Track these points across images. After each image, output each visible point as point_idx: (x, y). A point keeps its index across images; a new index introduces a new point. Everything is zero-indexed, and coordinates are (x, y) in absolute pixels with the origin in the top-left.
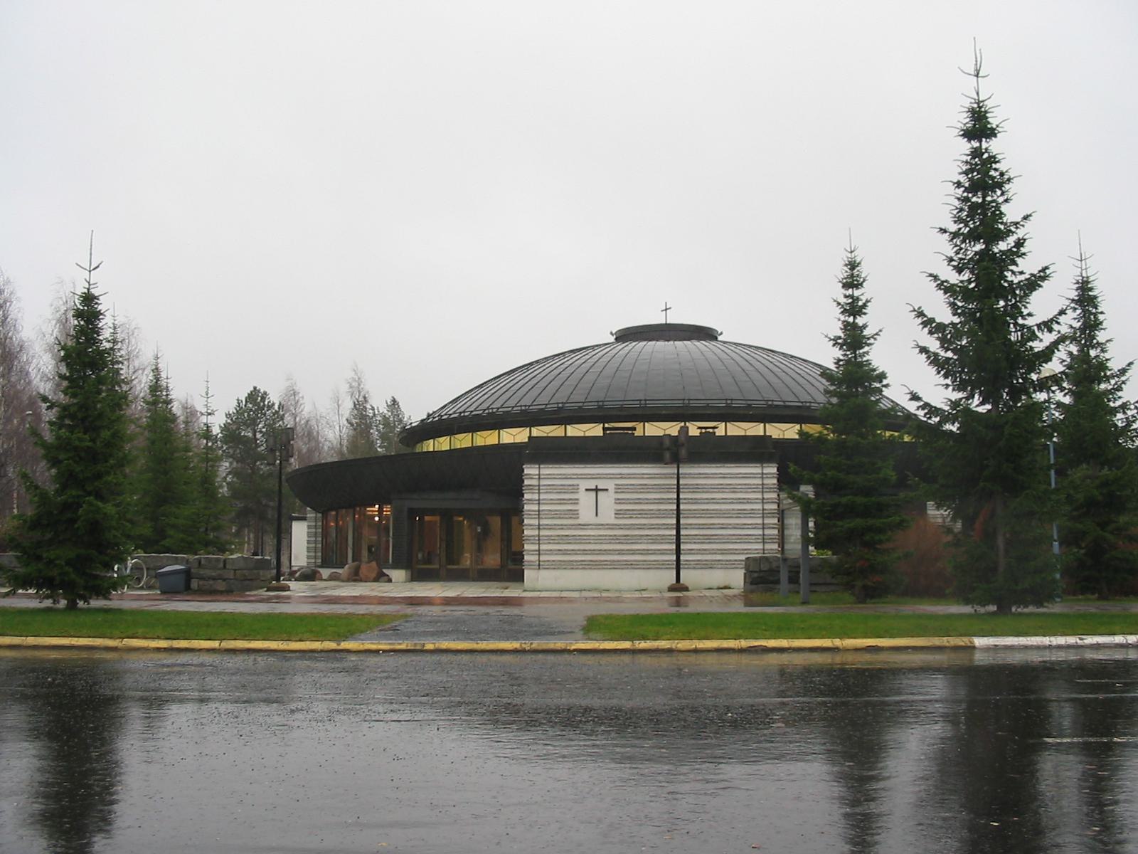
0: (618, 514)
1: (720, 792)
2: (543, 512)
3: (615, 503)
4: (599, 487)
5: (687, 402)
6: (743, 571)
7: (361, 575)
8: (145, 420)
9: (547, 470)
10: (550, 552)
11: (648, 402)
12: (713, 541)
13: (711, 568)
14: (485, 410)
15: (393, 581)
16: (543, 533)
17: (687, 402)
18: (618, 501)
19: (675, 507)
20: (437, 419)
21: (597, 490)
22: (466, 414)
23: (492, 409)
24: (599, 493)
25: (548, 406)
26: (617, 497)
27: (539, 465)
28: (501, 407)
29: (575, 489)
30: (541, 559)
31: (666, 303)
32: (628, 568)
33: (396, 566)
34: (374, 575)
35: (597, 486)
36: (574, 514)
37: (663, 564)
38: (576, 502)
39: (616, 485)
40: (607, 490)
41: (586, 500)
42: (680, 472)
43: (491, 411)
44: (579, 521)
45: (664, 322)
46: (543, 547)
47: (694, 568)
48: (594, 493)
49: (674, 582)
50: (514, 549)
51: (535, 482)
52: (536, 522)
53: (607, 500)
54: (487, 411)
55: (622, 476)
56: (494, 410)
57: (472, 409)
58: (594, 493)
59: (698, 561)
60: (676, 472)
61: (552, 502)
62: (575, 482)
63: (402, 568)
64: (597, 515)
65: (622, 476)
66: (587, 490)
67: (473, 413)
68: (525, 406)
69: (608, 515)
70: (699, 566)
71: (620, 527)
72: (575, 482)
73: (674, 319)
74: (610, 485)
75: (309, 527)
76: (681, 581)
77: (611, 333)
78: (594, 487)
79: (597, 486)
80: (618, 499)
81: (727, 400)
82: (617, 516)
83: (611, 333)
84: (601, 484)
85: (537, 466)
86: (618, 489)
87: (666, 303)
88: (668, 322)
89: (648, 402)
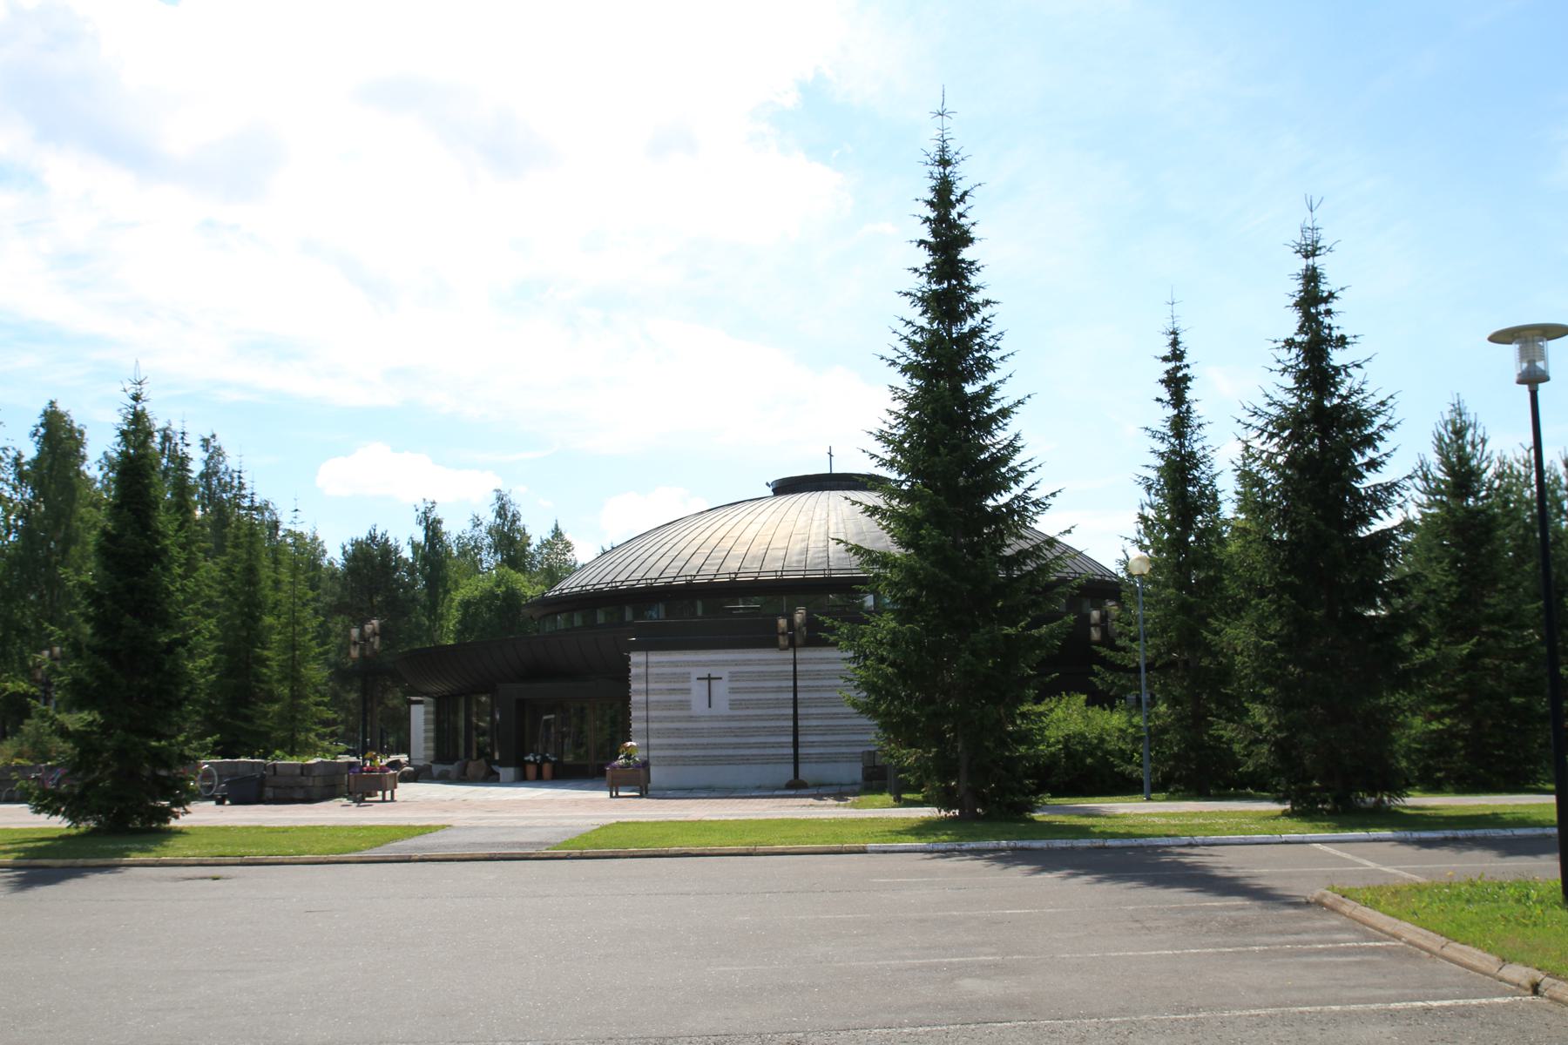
0: (734, 704)
1: (1331, 898)
3: (730, 692)
4: (712, 676)
6: (861, 765)
7: (469, 774)
8: (78, 599)
9: (655, 657)
11: (833, 572)
12: (836, 732)
13: (835, 762)
14: (609, 583)
15: (501, 780)
18: (733, 690)
19: (791, 696)
20: (558, 593)
21: (709, 679)
22: (588, 588)
23: (616, 582)
24: (713, 682)
25: (697, 578)
26: (731, 686)
28: (597, 584)
29: (686, 677)
31: (1521, 444)
32: (743, 764)
33: (502, 763)
34: (482, 773)
35: (709, 675)
36: (685, 705)
37: (783, 759)
38: (688, 691)
39: (730, 673)
40: (721, 678)
41: (698, 690)
42: (797, 656)
43: (614, 585)
44: (692, 713)
45: (829, 472)
47: (816, 762)
49: (792, 777)
50: (298, 771)
53: (720, 689)
54: (610, 585)
55: (736, 663)
56: (618, 584)
57: (623, 579)
58: (707, 681)
59: (821, 754)
60: (792, 657)
61: (661, 692)
62: (687, 670)
63: (511, 766)
64: (710, 706)
65: (736, 663)
66: (698, 679)
67: (596, 587)
68: (651, 579)
69: (722, 706)
70: (821, 760)
71: (740, 718)
72: (687, 670)
73: (838, 469)
74: (723, 672)
75: (426, 713)
76: (800, 776)
77: (767, 484)
79: (709, 675)
80: (733, 688)
81: (730, 573)
83: (767, 484)
86: (734, 677)
87: (1521, 444)
88: (833, 472)
89: (833, 572)
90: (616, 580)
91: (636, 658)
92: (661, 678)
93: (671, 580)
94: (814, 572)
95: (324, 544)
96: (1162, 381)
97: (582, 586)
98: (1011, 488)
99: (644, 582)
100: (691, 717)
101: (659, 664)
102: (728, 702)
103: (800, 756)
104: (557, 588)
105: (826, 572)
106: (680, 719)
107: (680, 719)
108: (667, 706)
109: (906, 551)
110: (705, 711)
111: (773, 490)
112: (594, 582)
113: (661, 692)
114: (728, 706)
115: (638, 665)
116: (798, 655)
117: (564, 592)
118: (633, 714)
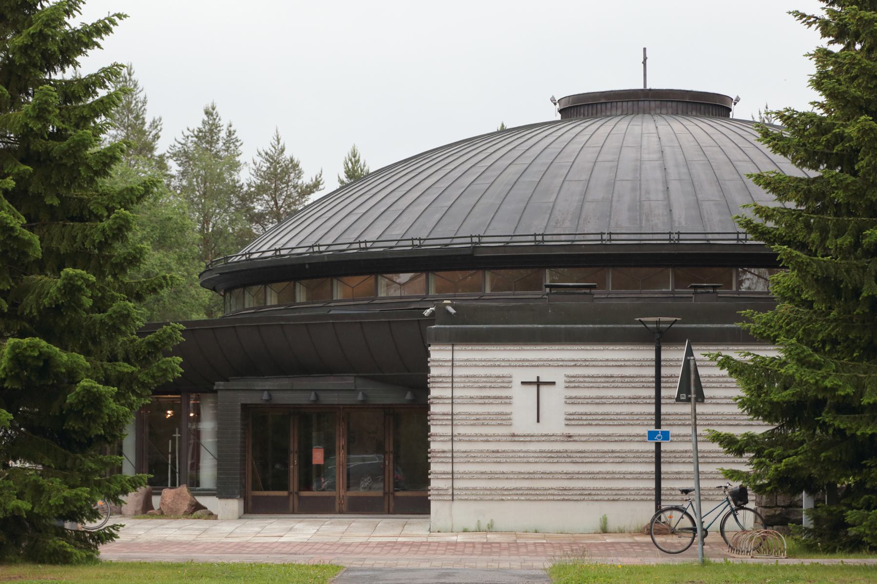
0: (571, 419)
2: (460, 417)
3: (566, 403)
4: (541, 380)
5: (676, 237)
9: (464, 353)
10: (471, 476)
16: (458, 447)
17: (676, 237)
18: (571, 401)
20: (244, 258)
21: (538, 383)
22: (283, 252)
24: (543, 389)
27: (453, 345)
29: (505, 382)
30: (455, 470)
35: (538, 378)
36: (504, 419)
41: (523, 398)
44: (514, 430)
45: (642, 87)
46: (458, 468)
48: (535, 388)
50: (745, 475)
51: (446, 372)
52: (447, 430)
55: (575, 363)
57: (329, 242)
61: (471, 400)
64: (538, 421)
65: (575, 363)
66: (523, 383)
73: (654, 84)
78: (536, 380)
79: (538, 378)
82: (568, 422)
83: (553, 100)
84: (546, 375)
85: (450, 348)
86: (572, 382)
88: (652, 85)
90: (321, 243)
91: (438, 354)
92: (472, 381)
93: (393, 244)
94: (650, 237)
95: (300, 166)
96: (112, 32)
97: (276, 250)
98: (239, 161)
99: (357, 246)
100: (514, 435)
101: (468, 364)
102: (513, 422)
103: (653, 498)
104: (246, 250)
105: (605, 237)
106: (498, 438)
107: (498, 438)
108: (479, 420)
109: (797, 206)
110: (533, 429)
111: (560, 111)
112: (292, 244)
113: (471, 400)
114: (564, 422)
115: (440, 363)
116: (664, 356)
117: (252, 257)
118: (433, 430)
